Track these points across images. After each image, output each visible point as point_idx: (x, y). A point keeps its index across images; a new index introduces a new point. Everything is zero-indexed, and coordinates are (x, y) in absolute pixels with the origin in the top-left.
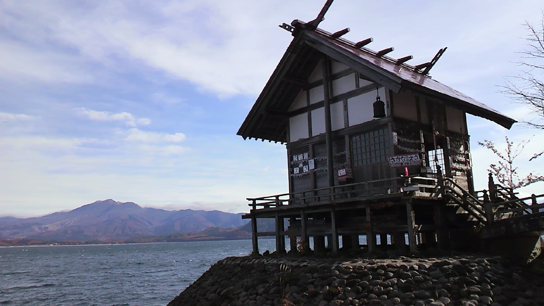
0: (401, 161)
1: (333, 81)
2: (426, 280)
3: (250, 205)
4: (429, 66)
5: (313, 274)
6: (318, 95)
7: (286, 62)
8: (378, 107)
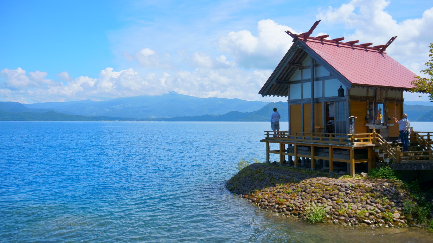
4: (385, 47)
6: (307, 74)
7: (272, 79)
8: (341, 91)
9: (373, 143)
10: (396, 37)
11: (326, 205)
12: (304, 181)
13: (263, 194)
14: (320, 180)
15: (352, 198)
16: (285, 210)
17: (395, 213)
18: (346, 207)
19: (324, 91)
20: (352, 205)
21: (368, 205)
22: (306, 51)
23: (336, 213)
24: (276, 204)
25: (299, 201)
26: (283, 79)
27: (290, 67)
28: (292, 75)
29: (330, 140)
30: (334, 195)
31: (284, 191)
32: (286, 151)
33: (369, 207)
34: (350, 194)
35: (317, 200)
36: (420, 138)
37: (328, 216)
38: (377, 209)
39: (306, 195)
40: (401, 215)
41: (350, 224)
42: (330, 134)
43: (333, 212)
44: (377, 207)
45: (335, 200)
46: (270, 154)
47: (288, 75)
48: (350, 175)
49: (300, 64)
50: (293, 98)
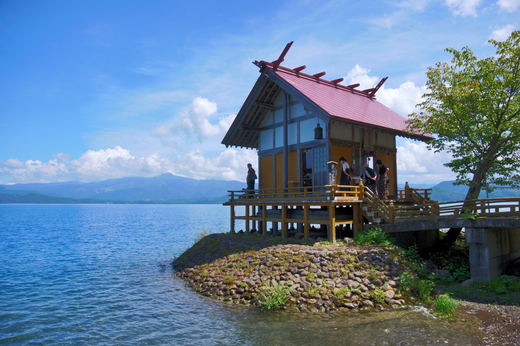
4: (374, 91)
7: (237, 124)
8: (319, 131)
9: (359, 199)
10: (387, 78)
11: (292, 283)
12: (265, 249)
13: (210, 270)
14: (287, 248)
15: (329, 271)
16: (234, 291)
17: (387, 290)
18: (319, 284)
19: (299, 135)
20: (328, 282)
21: (351, 281)
22: (276, 82)
23: (305, 293)
24: (223, 283)
25: (255, 279)
26: (251, 124)
27: (259, 107)
28: (262, 119)
29: (305, 195)
31: (238, 264)
33: (351, 283)
34: (326, 266)
35: (280, 275)
37: (293, 299)
38: (363, 286)
39: (265, 269)
40: (396, 293)
41: (323, 309)
43: (300, 293)
44: (362, 282)
45: (305, 275)
46: (236, 220)
47: (257, 118)
48: (329, 241)
49: (272, 104)
50: (262, 149)
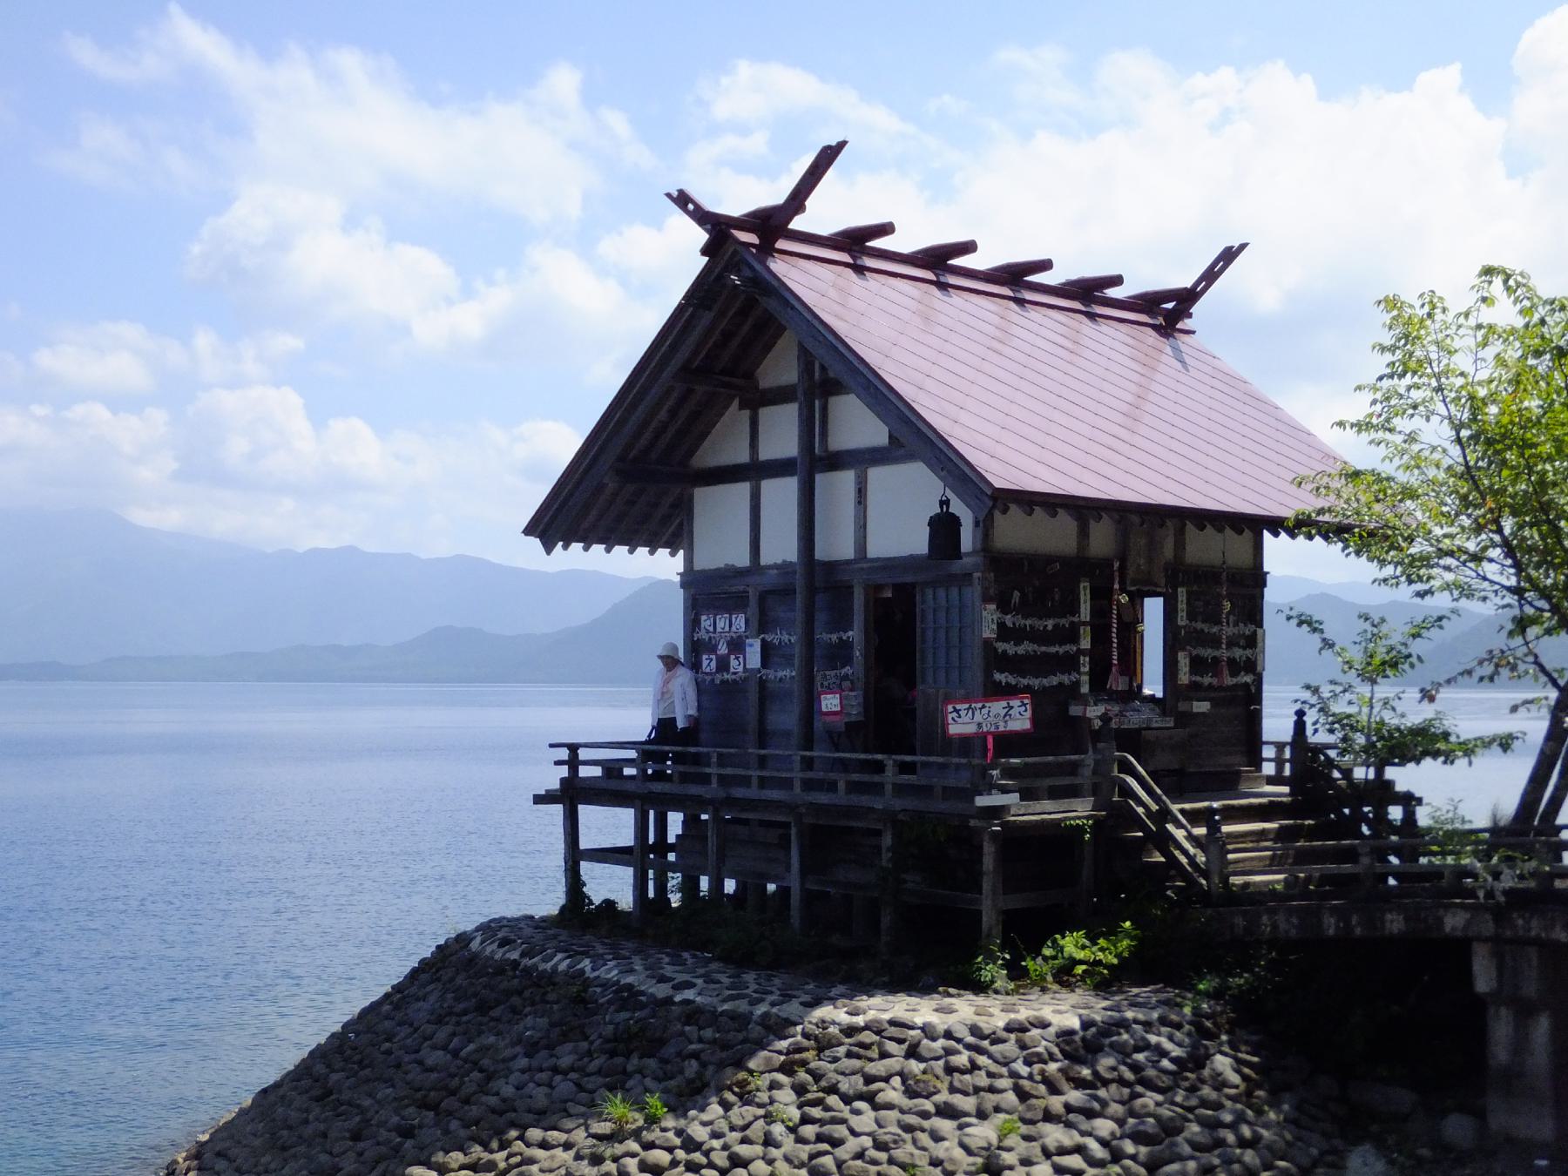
0: (978, 718)
1: (833, 400)
2: (974, 1067)
3: (558, 763)
4: (1186, 298)
5: (700, 1029)
6: (781, 434)
8: (944, 527)
22: (771, 304)
27: (690, 391)
30: (886, 1080)
32: (672, 848)
36: (1336, 774)
41: (892, 1093)
42: (889, 761)
46: (585, 866)
50: (703, 562)
